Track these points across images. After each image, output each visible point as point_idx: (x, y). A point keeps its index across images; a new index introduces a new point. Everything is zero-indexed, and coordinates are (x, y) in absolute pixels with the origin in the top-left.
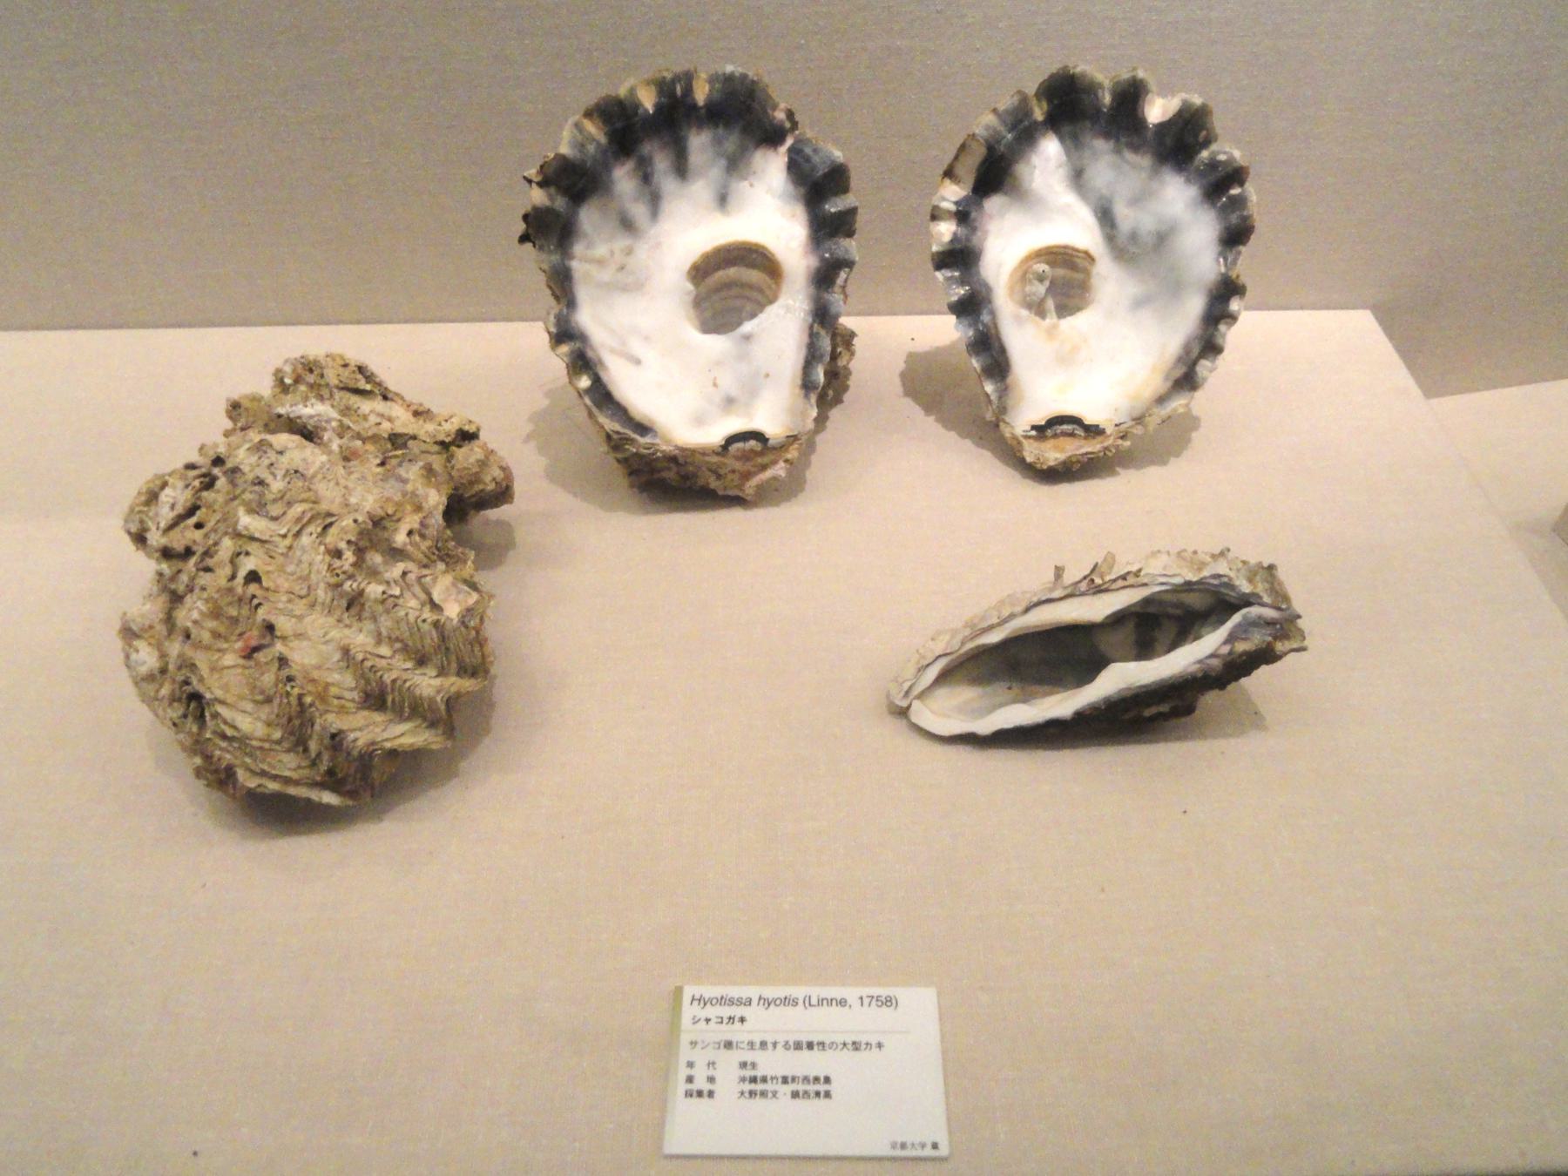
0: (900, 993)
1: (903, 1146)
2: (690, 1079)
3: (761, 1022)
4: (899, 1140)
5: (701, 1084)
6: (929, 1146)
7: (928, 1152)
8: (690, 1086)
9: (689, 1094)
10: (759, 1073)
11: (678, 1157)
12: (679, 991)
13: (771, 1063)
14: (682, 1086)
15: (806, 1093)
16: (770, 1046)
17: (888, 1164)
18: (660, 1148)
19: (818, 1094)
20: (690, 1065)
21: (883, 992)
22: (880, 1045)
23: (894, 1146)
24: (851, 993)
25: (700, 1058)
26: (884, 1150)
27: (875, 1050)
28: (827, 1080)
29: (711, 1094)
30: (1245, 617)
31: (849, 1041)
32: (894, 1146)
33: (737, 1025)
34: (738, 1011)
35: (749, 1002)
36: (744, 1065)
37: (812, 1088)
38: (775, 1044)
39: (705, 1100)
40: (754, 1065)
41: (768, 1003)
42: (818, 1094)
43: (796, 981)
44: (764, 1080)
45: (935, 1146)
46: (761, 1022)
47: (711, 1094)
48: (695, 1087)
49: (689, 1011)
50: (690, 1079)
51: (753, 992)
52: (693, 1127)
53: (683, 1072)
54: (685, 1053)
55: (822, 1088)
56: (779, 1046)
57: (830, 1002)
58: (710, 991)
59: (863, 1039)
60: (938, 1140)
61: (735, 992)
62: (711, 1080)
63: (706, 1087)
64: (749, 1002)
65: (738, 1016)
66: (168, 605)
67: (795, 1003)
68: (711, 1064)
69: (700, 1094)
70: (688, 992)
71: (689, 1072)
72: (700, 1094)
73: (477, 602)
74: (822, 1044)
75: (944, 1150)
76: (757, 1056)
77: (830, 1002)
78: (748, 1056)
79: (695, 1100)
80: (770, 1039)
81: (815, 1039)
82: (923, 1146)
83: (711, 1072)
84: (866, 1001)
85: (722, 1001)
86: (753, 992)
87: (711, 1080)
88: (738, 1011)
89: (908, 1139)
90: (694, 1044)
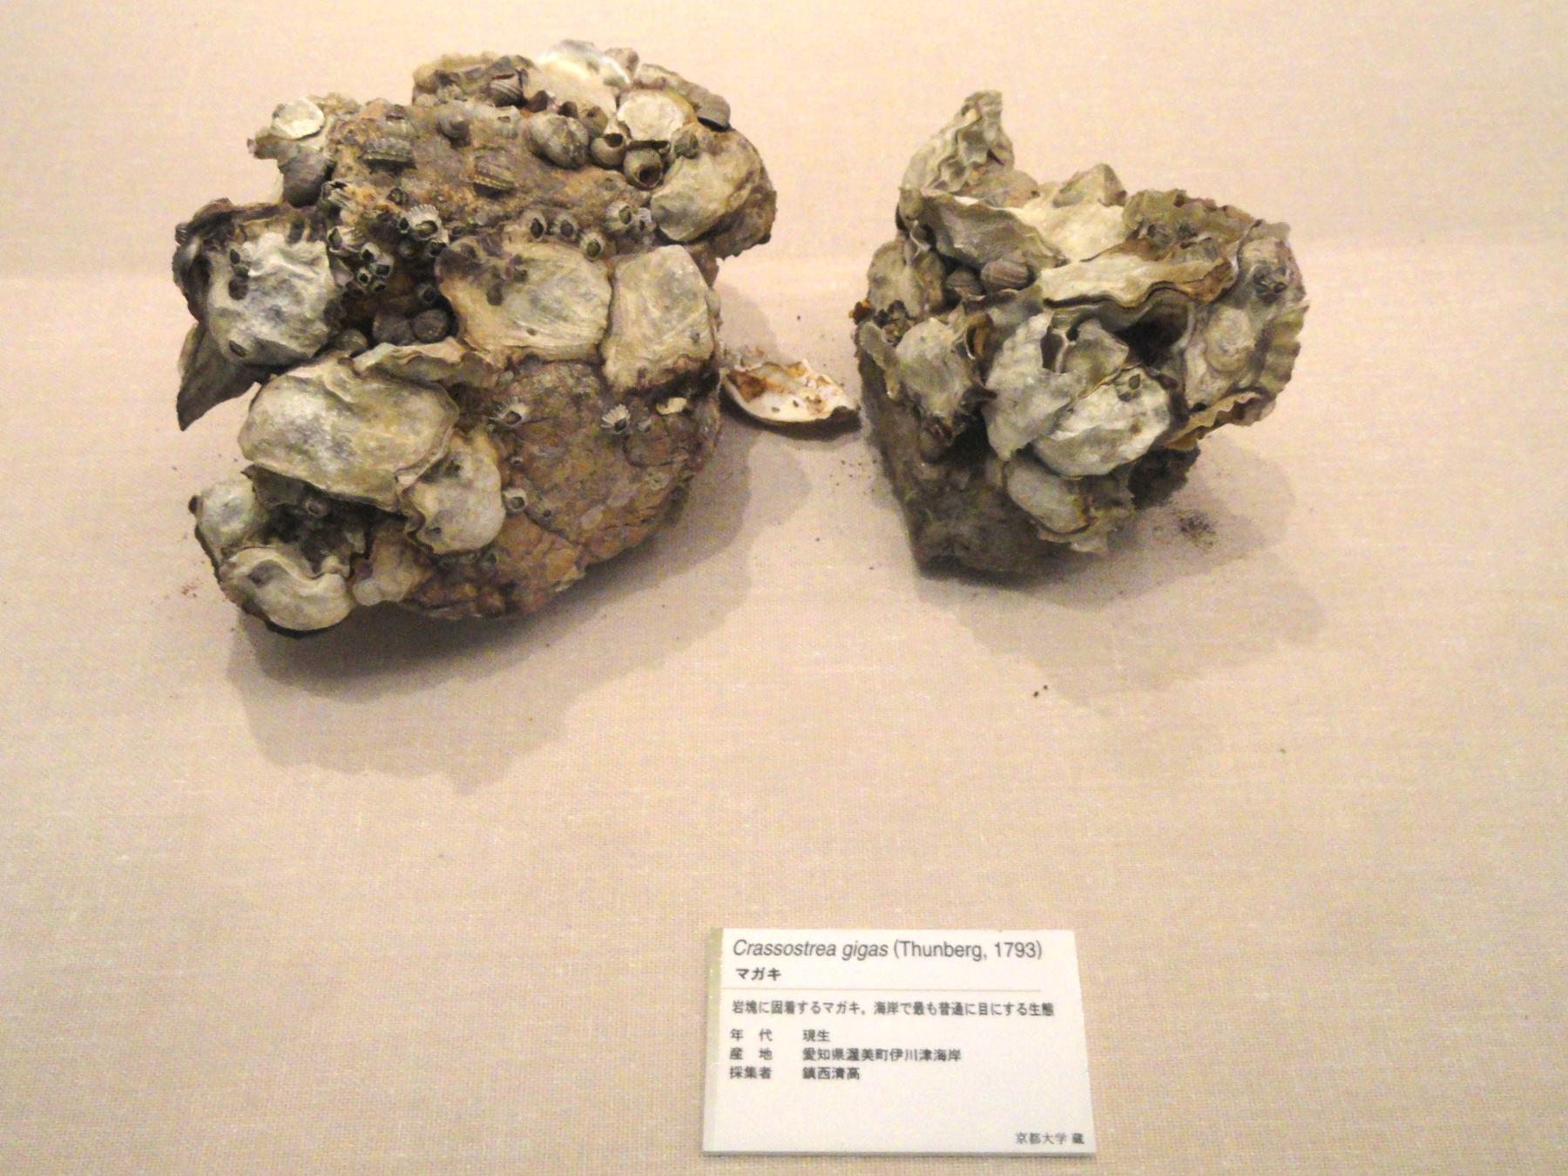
0: (1044, 936)
1: (1034, 1138)
2: (736, 1054)
3: (799, 977)
4: (1028, 1131)
5: (751, 1059)
7: (1069, 1147)
8: (736, 1063)
9: (735, 1073)
11: (720, 1156)
12: (717, 935)
13: (845, 1033)
14: (726, 1063)
15: (823, 1070)
16: (797, 1009)
17: (860, 1164)
18: (700, 1145)
19: (840, 1073)
20: (737, 1034)
21: (1024, 936)
23: (1021, 1138)
24: (985, 939)
25: (745, 1021)
26: (1013, 1147)
28: (809, 1074)
29: (766, 1073)
31: (1039, 1002)
32: (1021, 1138)
33: (767, 980)
34: (767, 963)
36: (810, 1035)
37: (834, 1064)
38: (802, 1005)
39: (759, 1081)
40: (823, 1035)
42: (840, 1073)
43: (922, 925)
45: (1078, 1139)
46: (799, 977)
47: (766, 1073)
48: (743, 1063)
49: (729, 963)
50: (736, 1054)
52: (740, 1117)
53: (728, 1044)
54: (729, 1020)
55: (816, 1064)
56: (808, 1008)
57: (959, 951)
59: (797, 999)
62: (766, 1054)
63: (759, 1063)
67: (832, 951)
68: (765, 1033)
69: (750, 1072)
70: (730, 936)
71: (736, 1044)
72: (750, 1072)
73: (1128, 518)
75: (1088, 1147)
77: (959, 951)
78: (816, 1023)
79: (743, 1082)
80: (797, 1000)
82: (1062, 1138)
83: (765, 1044)
84: (1004, 949)
87: (766, 1054)
88: (767, 963)
89: (1040, 1130)
90: (737, 1007)
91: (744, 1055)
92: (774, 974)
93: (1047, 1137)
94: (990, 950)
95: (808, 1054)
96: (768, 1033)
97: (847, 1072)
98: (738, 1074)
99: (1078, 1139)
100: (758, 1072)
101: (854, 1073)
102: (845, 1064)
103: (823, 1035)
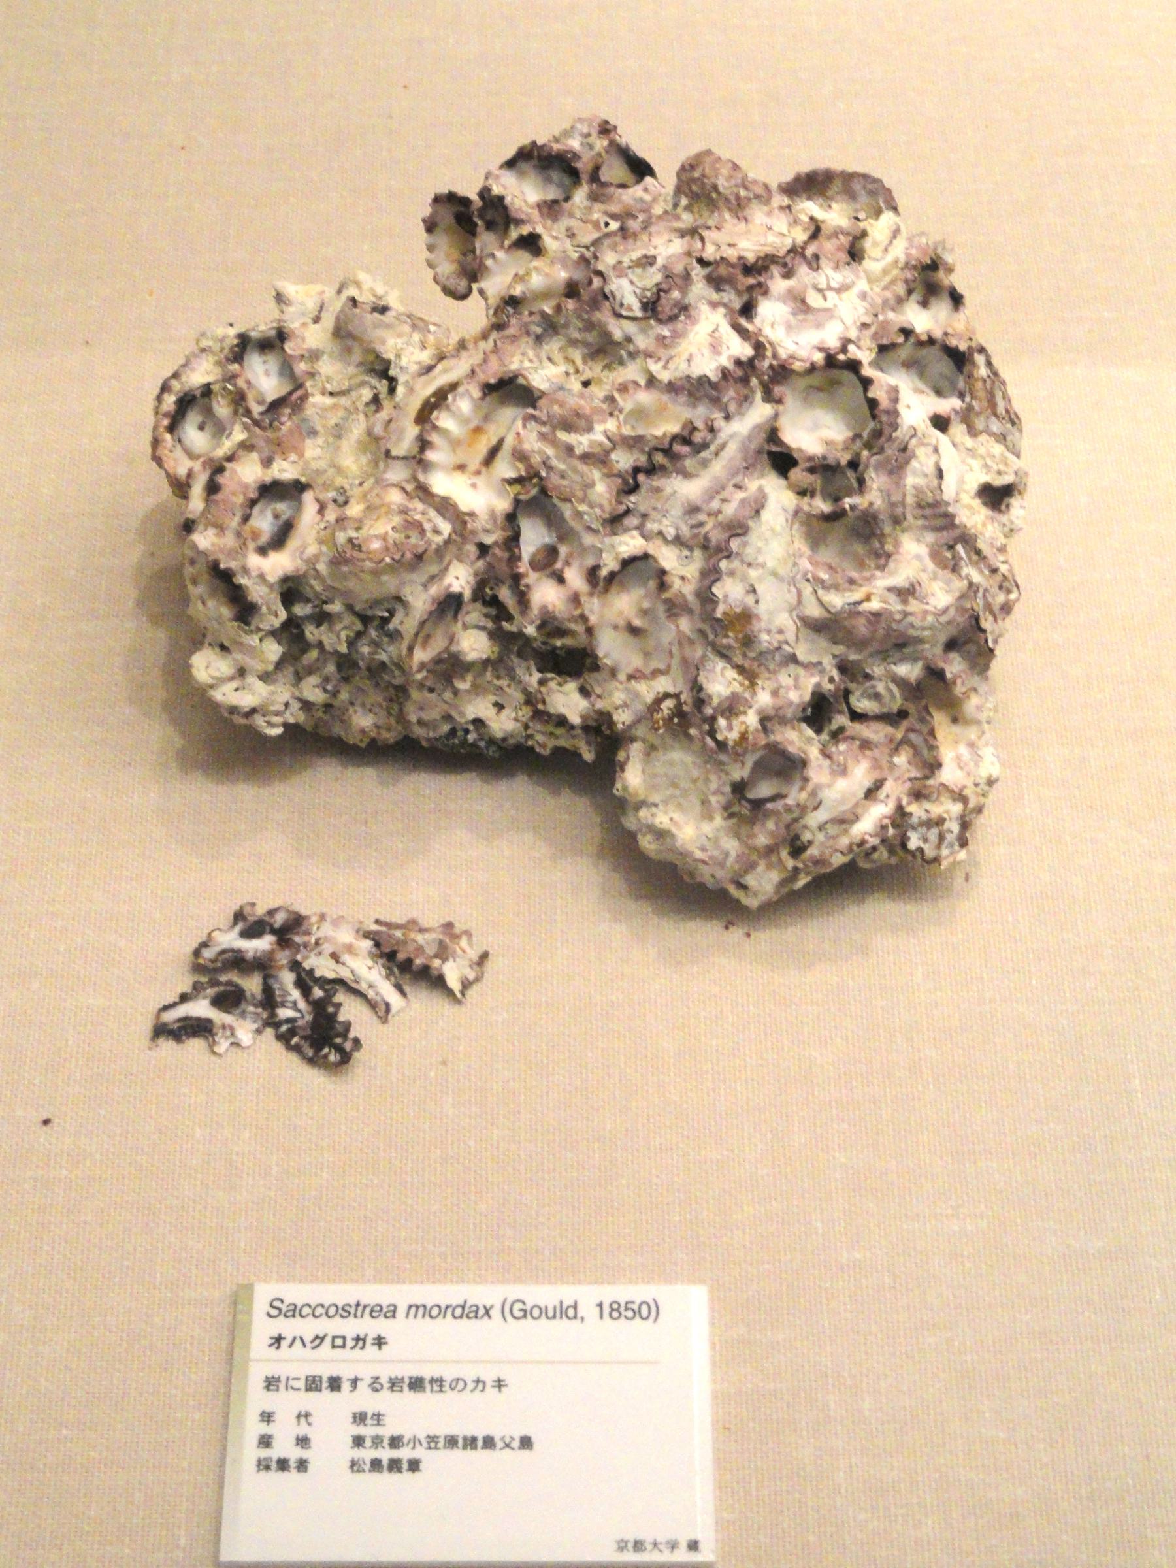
1: (638, 1545)
2: (266, 1441)
4: (631, 1537)
5: (284, 1447)
6: (683, 1545)
8: (264, 1453)
9: (264, 1465)
10: (386, 1432)
12: (240, 1299)
13: (408, 1415)
14: (252, 1453)
16: (346, 1386)
20: (267, 1417)
21: (637, 1293)
22: (500, 1384)
23: (622, 1546)
24: (587, 1296)
25: (286, 1404)
27: (491, 1392)
29: (302, 1465)
30: (961, 558)
32: (622, 1546)
35: (392, 1312)
36: (360, 1418)
38: (355, 1382)
39: (293, 1475)
40: (378, 1418)
41: (417, 1309)
42: (376, 1465)
43: (536, 1276)
44: (395, 1442)
45: (693, 1546)
46: (413, 1345)
48: (275, 1453)
49: (262, 1328)
50: (266, 1441)
51: (401, 1295)
53: (254, 1428)
54: (257, 1399)
58: (296, 1293)
60: (699, 1537)
61: (373, 1294)
62: (303, 1442)
63: (294, 1453)
64: (392, 1312)
65: (350, 1335)
66: (833, 610)
68: (304, 1416)
69: (283, 1465)
70: (264, 1294)
71: (264, 1429)
72: (283, 1465)
74: (438, 1382)
75: (705, 1555)
76: (384, 1402)
78: (364, 1400)
79: (275, 1476)
81: (427, 1372)
82: (673, 1545)
83: (303, 1430)
85: (344, 1311)
86: (401, 1295)
87: (303, 1442)
88: (378, 1327)
89: (647, 1536)
90: (271, 1383)
91: (275, 1443)
92: (380, 1342)
93: (655, 1544)
94: (587, 1309)
95: (358, 1441)
96: (307, 1415)
97: (264, 1429)
98: (268, 1468)
99: (693, 1546)
100: (292, 1464)
101: (414, 1465)
102: (405, 1454)
103: (378, 1418)
